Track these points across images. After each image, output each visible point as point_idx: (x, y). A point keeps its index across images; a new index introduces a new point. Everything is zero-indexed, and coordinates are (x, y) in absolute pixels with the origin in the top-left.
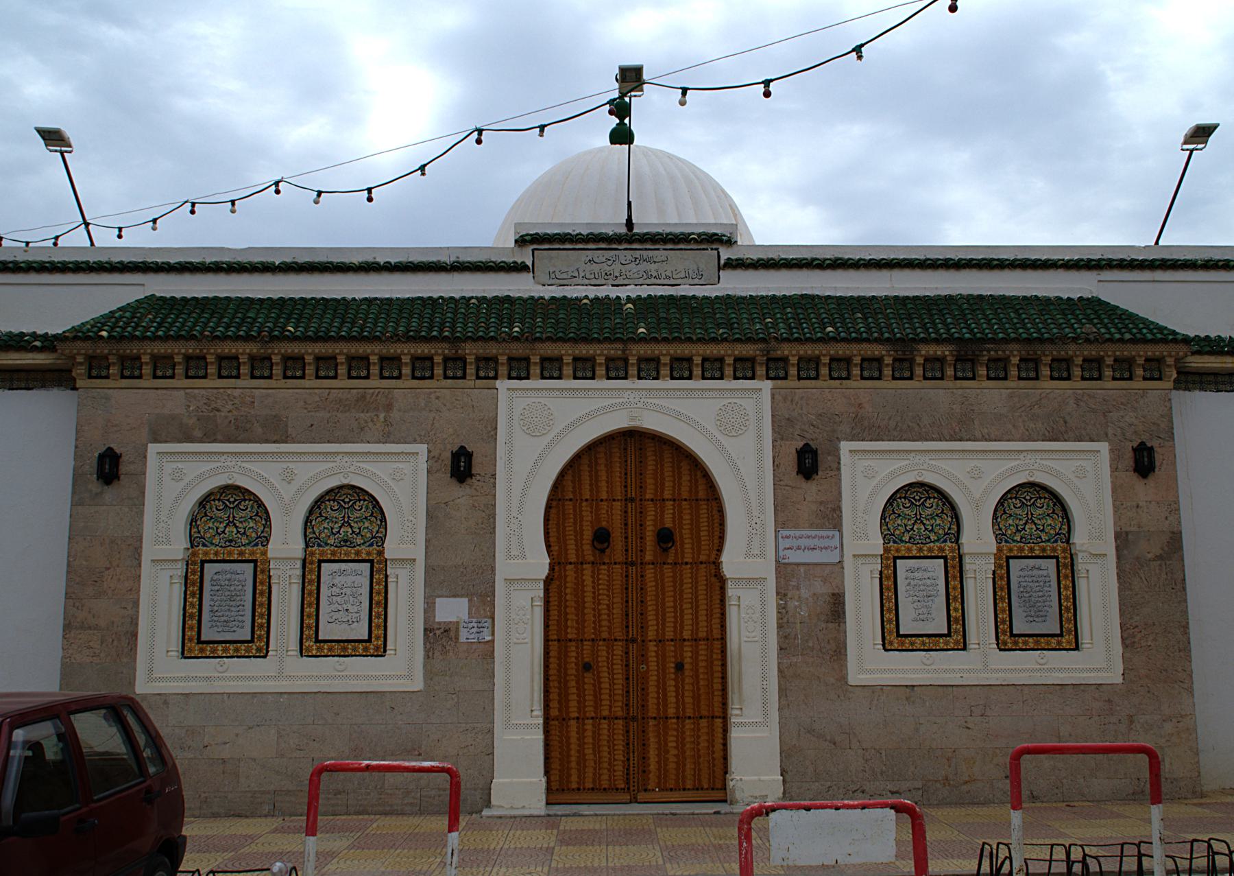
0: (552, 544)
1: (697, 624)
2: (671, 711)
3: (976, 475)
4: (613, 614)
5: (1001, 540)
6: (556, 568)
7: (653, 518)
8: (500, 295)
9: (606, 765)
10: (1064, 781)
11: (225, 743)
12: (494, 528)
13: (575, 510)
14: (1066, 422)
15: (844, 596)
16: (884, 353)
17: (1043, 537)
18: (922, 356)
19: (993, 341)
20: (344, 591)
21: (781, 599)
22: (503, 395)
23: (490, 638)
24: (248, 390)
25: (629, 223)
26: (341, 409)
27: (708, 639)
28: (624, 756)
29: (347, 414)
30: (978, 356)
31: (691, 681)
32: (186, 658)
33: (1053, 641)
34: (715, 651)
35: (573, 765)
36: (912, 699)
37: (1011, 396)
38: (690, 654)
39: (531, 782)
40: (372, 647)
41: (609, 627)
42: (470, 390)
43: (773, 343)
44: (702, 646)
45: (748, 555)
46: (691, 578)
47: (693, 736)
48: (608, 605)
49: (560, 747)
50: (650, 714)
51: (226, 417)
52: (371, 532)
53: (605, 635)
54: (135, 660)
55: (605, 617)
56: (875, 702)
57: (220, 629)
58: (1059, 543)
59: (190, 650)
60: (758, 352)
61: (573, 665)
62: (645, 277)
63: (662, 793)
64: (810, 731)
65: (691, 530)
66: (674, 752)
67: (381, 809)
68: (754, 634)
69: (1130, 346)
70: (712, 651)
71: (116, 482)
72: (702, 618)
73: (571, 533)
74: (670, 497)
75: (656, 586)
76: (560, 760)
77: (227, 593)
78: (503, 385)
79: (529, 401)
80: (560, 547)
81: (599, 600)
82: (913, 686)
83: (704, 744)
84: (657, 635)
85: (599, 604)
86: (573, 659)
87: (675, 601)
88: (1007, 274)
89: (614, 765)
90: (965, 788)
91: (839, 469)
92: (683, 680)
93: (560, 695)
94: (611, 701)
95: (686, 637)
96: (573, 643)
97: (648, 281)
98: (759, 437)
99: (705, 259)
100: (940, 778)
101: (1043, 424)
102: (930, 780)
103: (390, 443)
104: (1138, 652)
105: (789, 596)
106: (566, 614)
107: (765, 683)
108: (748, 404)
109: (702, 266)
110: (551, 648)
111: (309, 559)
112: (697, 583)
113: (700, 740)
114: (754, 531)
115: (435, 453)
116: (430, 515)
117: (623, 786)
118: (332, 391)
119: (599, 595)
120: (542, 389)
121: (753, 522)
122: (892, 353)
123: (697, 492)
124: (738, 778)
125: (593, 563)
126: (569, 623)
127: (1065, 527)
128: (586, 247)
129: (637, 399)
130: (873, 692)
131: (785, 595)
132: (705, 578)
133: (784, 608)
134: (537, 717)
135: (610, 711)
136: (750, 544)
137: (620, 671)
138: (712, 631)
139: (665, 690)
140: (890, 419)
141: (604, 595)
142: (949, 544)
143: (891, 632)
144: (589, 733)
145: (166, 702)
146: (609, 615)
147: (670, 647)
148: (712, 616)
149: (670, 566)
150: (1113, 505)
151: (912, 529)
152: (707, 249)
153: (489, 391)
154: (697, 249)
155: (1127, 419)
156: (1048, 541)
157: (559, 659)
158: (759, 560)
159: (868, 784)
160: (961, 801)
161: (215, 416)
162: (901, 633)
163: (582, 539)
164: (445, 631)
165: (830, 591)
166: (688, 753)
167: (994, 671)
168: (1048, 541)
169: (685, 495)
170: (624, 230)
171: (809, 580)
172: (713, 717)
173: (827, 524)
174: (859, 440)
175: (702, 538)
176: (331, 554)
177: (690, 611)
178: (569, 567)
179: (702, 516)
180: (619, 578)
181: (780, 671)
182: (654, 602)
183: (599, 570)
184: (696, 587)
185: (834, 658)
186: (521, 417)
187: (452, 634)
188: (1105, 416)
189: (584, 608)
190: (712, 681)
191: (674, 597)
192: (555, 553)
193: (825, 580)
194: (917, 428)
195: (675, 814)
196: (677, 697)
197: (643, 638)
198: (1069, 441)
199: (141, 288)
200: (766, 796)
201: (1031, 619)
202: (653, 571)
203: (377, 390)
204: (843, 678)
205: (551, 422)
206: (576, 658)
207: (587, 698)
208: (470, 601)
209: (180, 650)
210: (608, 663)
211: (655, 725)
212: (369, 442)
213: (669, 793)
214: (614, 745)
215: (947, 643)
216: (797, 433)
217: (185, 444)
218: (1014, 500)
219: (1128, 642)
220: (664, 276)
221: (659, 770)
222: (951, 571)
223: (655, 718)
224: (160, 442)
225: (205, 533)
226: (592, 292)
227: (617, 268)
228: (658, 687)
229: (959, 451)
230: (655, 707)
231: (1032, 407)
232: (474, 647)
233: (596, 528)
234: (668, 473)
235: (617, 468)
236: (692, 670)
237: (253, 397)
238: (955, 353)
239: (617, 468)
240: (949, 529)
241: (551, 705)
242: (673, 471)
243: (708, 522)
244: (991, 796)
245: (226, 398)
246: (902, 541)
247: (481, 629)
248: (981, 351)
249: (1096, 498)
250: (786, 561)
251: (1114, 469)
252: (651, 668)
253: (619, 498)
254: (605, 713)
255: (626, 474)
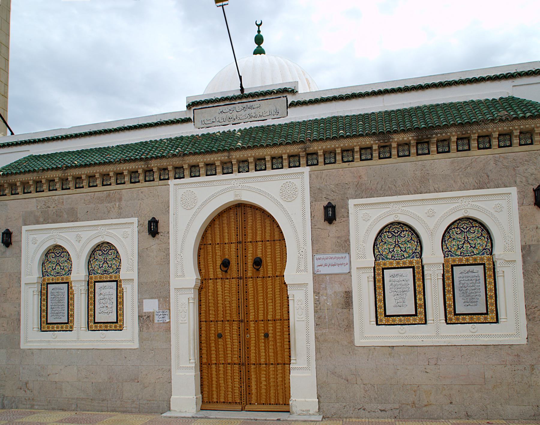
0: (202, 269)
1: (275, 311)
2: (263, 361)
3: (431, 214)
4: (232, 306)
5: (448, 255)
6: (204, 282)
7: (251, 252)
8: (178, 137)
9: (230, 390)
10: (488, 406)
11: (56, 374)
12: (169, 261)
13: (212, 250)
14: (488, 177)
15: (352, 293)
16: (372, 142)
17: (475, 252)
18: (395, 142)
19: (439, 127)
20: (105, 297)
21: (316, 296)
22: (172, 188)
23: (168, 321)
24: (61, 196)
25: (242, 89)
26: (100, 202)
27: (281, 320)
28: (239, 385)
29: (102, 205)
30: (430, 138)
31: (273, 344)
32: (42, 331)
33: (482, 317)
34: (285, 326)
35: (214, 389)
36: (392, 355)
37: (452, 163)
38: (272, 328)
39: (189, 398)
40: (118, 325)
41: (230, 314)
42: (157, 186)
43: (308, 143)
44: (278, 324)
45: (298, 270)
46: (272, 285)
47: (274, 374)
48: (229, 302)
49: (207, 379)
50: (252, 362)
51: (52, 210)
52: (116, 265)
53: (228, 318)
54: (20, 333)
55: (228, 308)
56: (371, 356)
57: (55, 317)
58: (485, 255)
59: (44, 328)
60: (300, 150)
61: (213, 335)
62: (249, 117)
63: (259, 406)
64: (334, 373)
65: (271, 258)
66: (264, 383)
67: (122, 409)
68: (302, 316)
69: (530, 121)
70: (283, 326)
71: (10, 246)
72: (278, 308)
73: (211, 262)
74: (260, 240)
75: (254, 290)
76: (208, 386)
77: (57, 299)
78: (172, 182)
79: (185, 190)
80: (206, 270)
81: (225, 299)
82: (393, 346)
83: (280, 379)
84: (255, 318)
85: (225, 301)
86: (213, 332)
87: (263, 299)
88: (454, 89)
89: (234, 390)
90: (425, 409)
91: (348, 216)
92: (268, 343)
93: (207, 351)
94: (232, 355)
95: (269, 319)
96: (213, 323)
97: (251, 120)
98: (303, 202)
99: (280, 103)
100: (410, 403)
101: (473, 178)
102: (404, 404)
103: (121, 218)
104: (537, 324)
105: (321, 293)
106: (209, 307)
107: (308, 345)
108: (297, 182)
109: (278, 107)
110: (202, 326)
111: (90, 281)
112: (275, 288)
113: (278, 377)
114: (301, 256)
115: (141, 222)
116: (140, 256)
117: (239, 401)
118: (96, 193)
119: (225, 296)
120: (191, 183)
121: (301, 251)
122: (377, 142)
123: (274, 236)
124: (294, 399)
125: (222, 279)
126: (211, 312)
127: (490, 244)
128: (219, 105)
129: (238, 184)
130: (369, 350)
131: (319, 293)
132: (279, 285)
133: (318, 301)
134: (192, 363)
135: (232, 360)
136: (299, 263)
137: (236, 338)
138: (283, 315)
139: (259, 348)
140: (377, 183)
141: (227, 296)
142: (415, 259)
143: (381, 314)
144: (221, 372)
145: (32, 353)
146: (230, 307)
147: (261, 324)
148: (283, 306)
149: (261, 279)
150: (520, 228)
151: (393, 251)
152: (281, 97)
153: (166, 186)
154: (276, 98)
155: (529, 170)
156: (478, 254)
157: (206, 331)
158: (304, 273)
159: (367, 405)
160: (422, 417)
161: (48, 210)
162: (457, 313)
163: (216, 266)
164: (148, 317)
165: (344, 290)
166: (272, 384)
167: (442, 337)
168: (478, 254)
169: (268, 238)
170: (239, 93)
171: (332, 284)
172: (284, 364)
173: (342, 250)
174: (360, 198)
175: (277, 262)
176: (99, 278)
177: (272, 304)
178: (210, 281)
179: (277, 250)
180: (235, 286)
181: (316, 338)
182: (253, 299)
183: (225, 282)
184: (275, 291)
185: (347, 330)
186: (181, 200)
187: (151, 318)
188: (514, 170)
189: (218, 303)
190: (284, 343)
191: (263, 296)
192: (203, 274)
193: (341, 283)
194: (394, 188)
195: (256, 420)
196: (265, 352)
197: (248, 320)
198: (490, 188)
199: (28, 152)
200: (309, 410)
201: (468, 304)
202: (252, 282)
203: (115, 191)
204: (352, 342)
205: (196, 201)
206: (215, 331)
207: (220, 353)
208: (159, 300)
209: (40, 327)
210: (230, 334)
211: (255, 368)
212: (112, 219)
213: (262, 406)
214: (234, 379)
215: (415, 320)
216: (324, 197)
217: (36, 225)
218: (456, 229)
219: (530, 317)
220: (258, 116)
221: (257, 393)
222: (417, 276)
223: (254, 364)
224: (27, 225)
225: (48, 269)
226: (222, 129)
227: (235, 114)
228: (255, 346)
229: (420, 200)
230: (254, 358)
231: (466, 168)
232: (161, 325)
233: (223, 259)
234: (259, 226)
235: (233, 225)
236: (273, 337)
237: (63, 199)
238: (415, 138)
239: (233, 225)
240: (416, 249)
241: (203, 357)
242: (262, 225)
243: (280, 253)
244: (441, 414)
245: (52, 201)
246: (387, 258)
247: (164, 316)
248: (432, 135)
249: (509, 224)
250: (319, 273)
251: (521, 204)
252: (252, 336)
253: (234, 242)
254: (229, 361)
255: (237, 228)
